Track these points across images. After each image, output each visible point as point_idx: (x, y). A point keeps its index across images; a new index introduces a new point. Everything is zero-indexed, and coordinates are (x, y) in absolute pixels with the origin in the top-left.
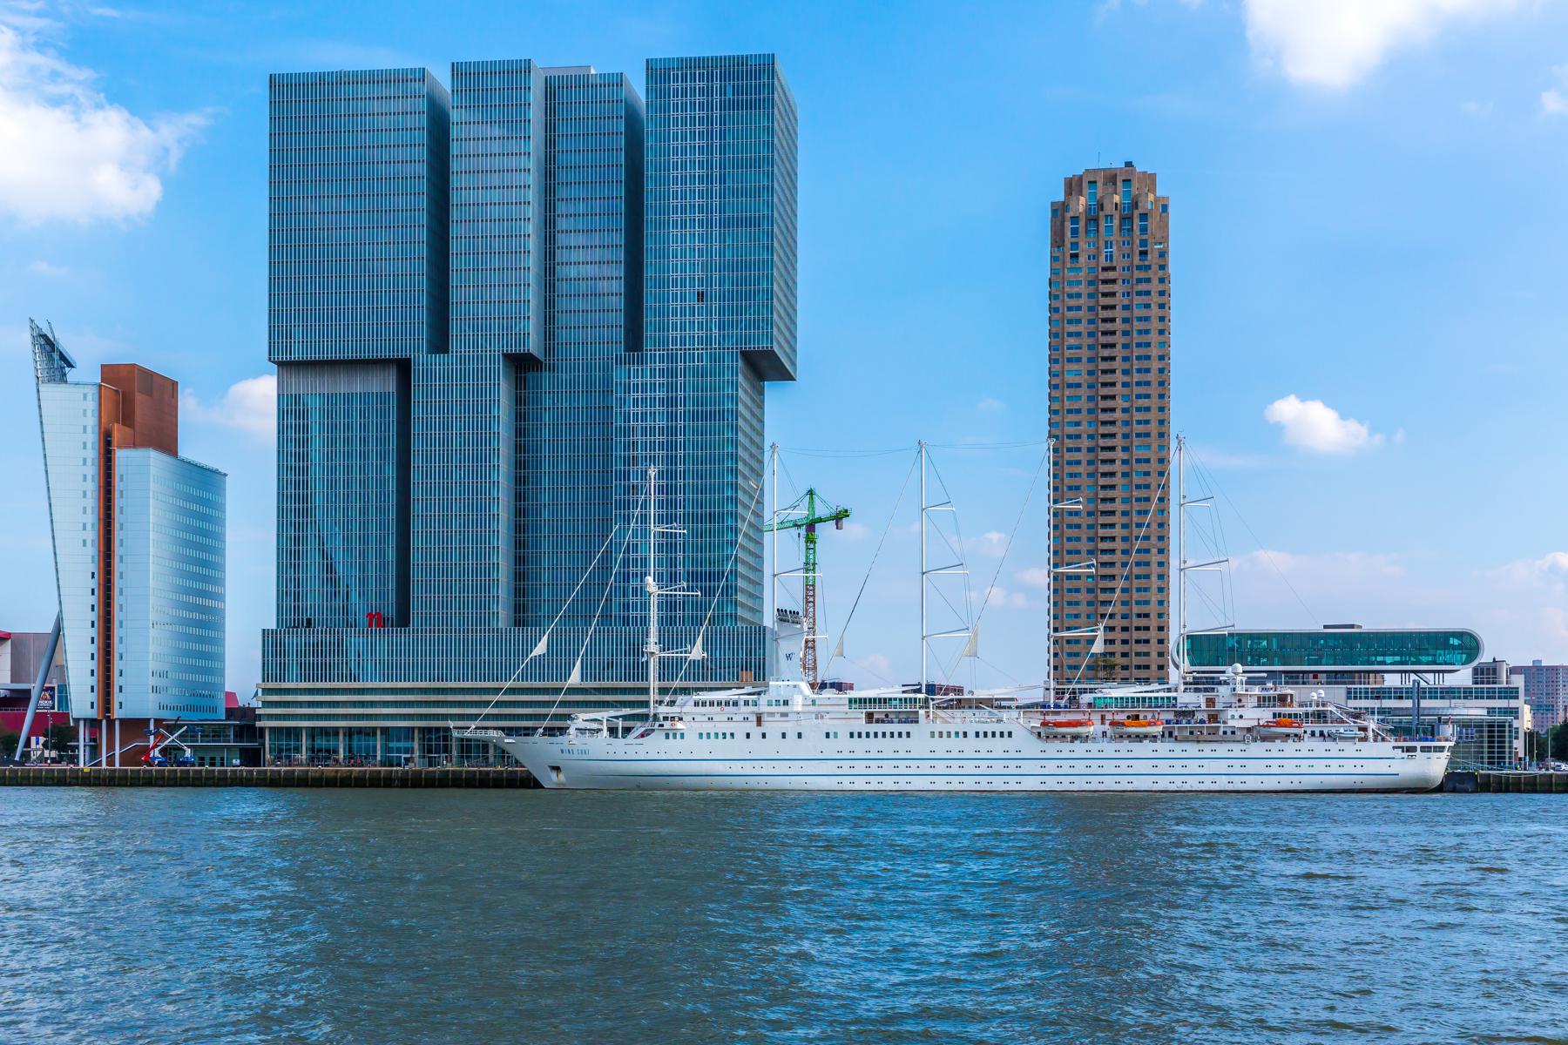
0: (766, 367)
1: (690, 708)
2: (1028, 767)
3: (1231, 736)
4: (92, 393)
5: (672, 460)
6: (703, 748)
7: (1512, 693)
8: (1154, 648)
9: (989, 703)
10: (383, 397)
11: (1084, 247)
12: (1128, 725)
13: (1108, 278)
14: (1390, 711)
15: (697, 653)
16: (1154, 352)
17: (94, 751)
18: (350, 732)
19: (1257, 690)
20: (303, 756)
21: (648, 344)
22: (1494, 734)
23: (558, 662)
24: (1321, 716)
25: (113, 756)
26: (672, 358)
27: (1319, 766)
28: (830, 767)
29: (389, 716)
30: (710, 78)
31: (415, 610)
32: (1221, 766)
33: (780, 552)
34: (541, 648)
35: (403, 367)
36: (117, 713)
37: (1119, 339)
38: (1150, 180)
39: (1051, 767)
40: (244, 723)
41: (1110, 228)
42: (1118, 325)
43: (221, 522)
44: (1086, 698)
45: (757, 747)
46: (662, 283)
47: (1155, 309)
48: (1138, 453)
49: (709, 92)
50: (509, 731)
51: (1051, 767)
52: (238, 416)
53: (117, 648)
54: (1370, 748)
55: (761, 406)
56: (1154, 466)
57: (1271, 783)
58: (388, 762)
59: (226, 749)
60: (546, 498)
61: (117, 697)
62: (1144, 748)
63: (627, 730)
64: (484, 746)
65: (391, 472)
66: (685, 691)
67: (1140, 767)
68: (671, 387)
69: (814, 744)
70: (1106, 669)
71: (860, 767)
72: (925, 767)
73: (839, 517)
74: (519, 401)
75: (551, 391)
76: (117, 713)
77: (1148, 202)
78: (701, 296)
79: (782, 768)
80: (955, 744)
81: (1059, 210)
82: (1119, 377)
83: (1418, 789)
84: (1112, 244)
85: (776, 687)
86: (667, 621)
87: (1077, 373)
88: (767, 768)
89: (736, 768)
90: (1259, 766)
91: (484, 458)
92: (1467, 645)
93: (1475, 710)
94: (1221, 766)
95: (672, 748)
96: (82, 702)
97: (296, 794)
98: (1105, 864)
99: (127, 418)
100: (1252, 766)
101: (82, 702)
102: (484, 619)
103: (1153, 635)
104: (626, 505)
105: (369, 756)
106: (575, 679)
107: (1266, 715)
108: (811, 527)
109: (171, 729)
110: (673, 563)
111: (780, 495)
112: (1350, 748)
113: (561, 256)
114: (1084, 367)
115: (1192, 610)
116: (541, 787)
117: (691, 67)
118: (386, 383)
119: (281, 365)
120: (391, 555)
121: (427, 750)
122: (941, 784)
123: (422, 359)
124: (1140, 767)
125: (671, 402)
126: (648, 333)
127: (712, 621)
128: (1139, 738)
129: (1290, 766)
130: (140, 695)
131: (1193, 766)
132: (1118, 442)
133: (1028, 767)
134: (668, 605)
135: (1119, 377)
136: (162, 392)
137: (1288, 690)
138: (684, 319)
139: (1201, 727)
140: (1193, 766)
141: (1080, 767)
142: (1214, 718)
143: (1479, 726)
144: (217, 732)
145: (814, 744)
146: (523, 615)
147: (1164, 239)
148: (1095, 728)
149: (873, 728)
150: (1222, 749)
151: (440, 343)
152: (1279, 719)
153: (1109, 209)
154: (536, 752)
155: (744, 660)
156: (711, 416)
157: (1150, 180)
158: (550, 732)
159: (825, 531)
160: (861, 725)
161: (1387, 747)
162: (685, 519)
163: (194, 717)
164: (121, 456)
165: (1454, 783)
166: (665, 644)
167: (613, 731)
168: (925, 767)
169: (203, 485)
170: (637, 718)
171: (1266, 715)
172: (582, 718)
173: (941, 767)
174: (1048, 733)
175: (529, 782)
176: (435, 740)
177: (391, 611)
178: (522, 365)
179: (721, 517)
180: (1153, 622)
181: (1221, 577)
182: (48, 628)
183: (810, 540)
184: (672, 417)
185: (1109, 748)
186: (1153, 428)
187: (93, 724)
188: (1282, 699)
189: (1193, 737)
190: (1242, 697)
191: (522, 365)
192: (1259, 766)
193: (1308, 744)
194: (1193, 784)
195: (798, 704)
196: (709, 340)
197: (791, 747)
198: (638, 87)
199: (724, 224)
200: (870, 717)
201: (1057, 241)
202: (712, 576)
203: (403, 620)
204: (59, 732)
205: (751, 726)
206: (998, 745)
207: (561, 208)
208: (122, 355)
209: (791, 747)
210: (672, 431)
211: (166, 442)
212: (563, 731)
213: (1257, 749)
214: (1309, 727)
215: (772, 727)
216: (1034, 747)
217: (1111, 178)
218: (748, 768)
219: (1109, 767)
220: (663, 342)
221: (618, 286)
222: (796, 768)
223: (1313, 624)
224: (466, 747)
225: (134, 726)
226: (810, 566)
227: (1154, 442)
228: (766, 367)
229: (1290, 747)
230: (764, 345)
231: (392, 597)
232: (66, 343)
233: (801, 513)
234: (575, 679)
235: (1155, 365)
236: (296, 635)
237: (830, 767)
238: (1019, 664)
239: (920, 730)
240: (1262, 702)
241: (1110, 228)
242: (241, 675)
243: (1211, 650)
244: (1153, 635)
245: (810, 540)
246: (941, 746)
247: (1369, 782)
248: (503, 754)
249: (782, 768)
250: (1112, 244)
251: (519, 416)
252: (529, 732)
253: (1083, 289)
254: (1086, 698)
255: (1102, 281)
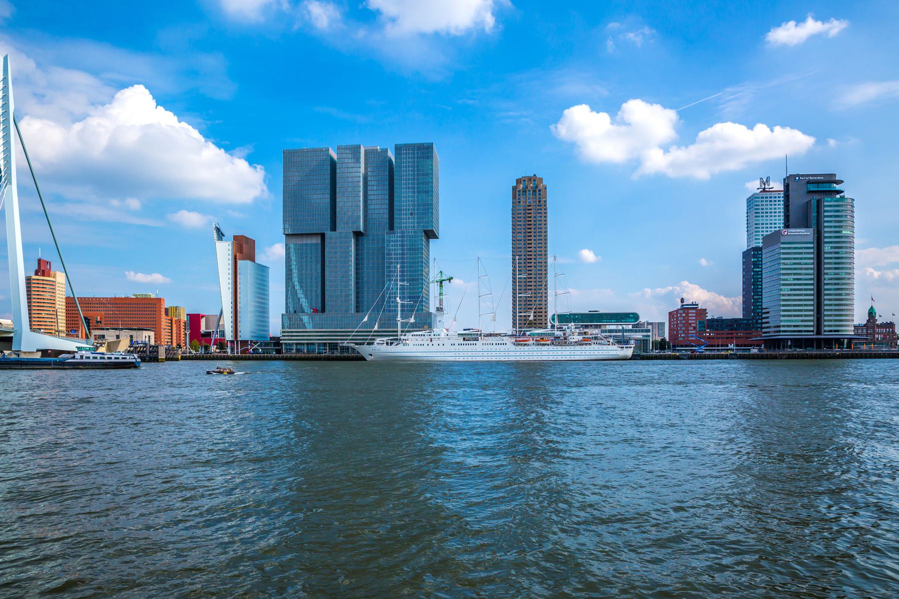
0: (430, 234)
1: (410, 337)
2: (511, 354)
3: (571, 344)
4: (230, 243)
5: (403, 263)
6: (415, 349)
7: (648, 331)
8: (544, 318)
9: (500, 335)
10: (317, 244)
11: (522, 200)
12: (541, 341)
13: (529, 207)
14: (616, 336)
15: (412, 320)
16: (543, 230)
17: (232, 350)
18: (308, 344)
19: (578, 330)
20: (294, 351)
21: (396, 229)
22: (643, 343)
23: (371, 323)
24: (596, 338)
25: (238, 352)
26: (403, 232)
27: (596, 353)
28: (452, 354)
29: (316, 340)
30: (414, 150)
31: (327, 307)
32: (568, 353)
33: (434, 289)
34: (366, 319)
35: (323, 236)
36: (239, 339)
37: (532, 226)
38: (541, 180)
39: (518, 354)
40: (276, 341)
41: (530, 194)
42: (532, 222)
43: (268, 282)
44: (528, 333)
45: (431, 348)
46: (400, 210)
47: (543, 218)
48: (538, 260)
49: (413, 154)
50: (356, 344)
51: (518, 354)
52: (274, 253)
53: (239, 319)
54: (611, 347)
55: (428, 246)
56: (543, 264)
57: (582, 358)
58: (319, 353)
59: (271, 350)
60: (365, 274)
61: (239, 334)
62: (545, 348)
63: (391, 344)
64: (348, 348)
65: (319, 266)
66: (409, 332)
67: (544, 353)
68: (402, 241)
69: (448, 347)
70: (531, 325)
71: (461, 354)
72: (481, 354)
73: (450, 279)
74: (357, 245)
75: (368, 245)
76: (239, 339)
77: (541, 187)
78: (411, 214)
79: (438, 354)
80: (490, 347)
81: (514, 189)
82: (533, 238)
83: (625, 359)
84: (530, 199)
85: (436, 330)
86: (402, 311)
87: (520, 236)
88: (434, 354)
89: (425, 354)
90: (579, 353)
91: (347, 262)
92: (635, 317)
93: (639, 336)
94: (568, 353)
95: (405, 349)
96: (229, 336)
97: (294, 363)
98: (529, 383)
99: (241, 252)
100: (577, 353)
101: (229, 336)
102: (347, 311)
103: (543, 314)
104: (389, 276)
105: (313, 351)
106: (376, 328)
107: (581, 338)
108: (441, 282)
109: (255, 343)
110: (403, 293)
111: (433, 274)
112: (605, 347)
113: (369, 202)
114: (523, 235)
115: (555, 307)
116: (365, 360)
117: (407, 146)
118: (317, 240)
119: (287, 235)
120: (319, 291)
121: (331, 349)
122: (461, 359)
123: (328, 233)
124: (544, 353)
125: (403, 245)
126: (396, 225)
127: (418, 310)
128: (544, 345)
129: (588, 353)
130: (246, 333)
131: (559, 353)
132: (533, 257)
133: (511, 354)
134: (403, 306)
135: (533, 238)
136: (251, 243)
137: (586, 330)
138: (406, 222)
139: (562, 341)
140: (559, 353)
141: (526, 353)
142: (565, 339)
143: (640, 340)
144: (267, 344)
145: (448, 347)
146: (358, 309)
147: (546, 197)
148: (531, 342)
149: (465, 342)
150: (568, 348)
151: (334, 228)
152: (585, 339)
153: (529, 188)
154: (364, 350)
155: (425, 323)
156: (415, 249)
157: (541, 180)
158: (368, 344)
159: (445, 283)
160: (462, 341)
161: (616, 347)
162: (407, 280)
163: (262, 340)
164: (239, 262)
165: (634, 357)
166: (403, 318)
167: (387, 344)
168: (481, 354)
169: (262, 271)
170: (395, 340)
171: (581, 338)
172: (378, 340)
173: (485, 354)
174: (517, 343)
175: (363, 359)
176: (333, 346)
177: (319, 308)
178: (358, 235)
179: (418, 280)
180: (543, 310)
181: (564, 296)
182: (219, 314)
183: (441, 286)
184: (403, 250)
185: (535, 348)
186: (543, 253)
187: (232, 342)
188: (585, 333)
189: (559, 344)
190: (573, 331)
191: (358, 235)
192: (579, 353)
193: (593, 346)
194: (560, 358)
195: (443, 335)
196: (414, 227)
197: (441, 348)
198: (391, 154)
199: (419, 192)
200: (464, 339)
201: (514, 197)
202: (416, 297)
203: (323, 310)
204: (221, 344)
205: (429, 342)
206: (502, 347)
207: (369, 188)
208: (239, 233)
209: (441, 348)
210: (403, 254)
211: (252, 258)
212: (373, 343)
213: (578, 348)
214: (593, 341)
215: (435, 342)
216: (513, 348)
217: (530, 179)
218: (428, 354)
219: (535, 353)
220: (400, 228)
221: (387, 211)
222: (442, 354)
223: (586, 311)
224: (343, 348)
225: (244, 343)
226: (441, 294)
227: (543, 256)
228: (430, 234)
229: (588, 347)
230: (430, 228)
231: (320, 305)
232: (223, 230)
233: (438, 279)
234: (376, 328)
235: (544, 234)
236: (292, 313)
237: (452, 354)
238: (505, 325)
239: (479, 343)
240: (580, 334)
241: (530, 194)
242: (275, 328)
243: (564, 318)
244: (543, 314)
245: (441, 286)
246: (485, 348)
247: (610, 357)
248: (353, 349)
249: (438, 354)
250: (530, 199)
251: (357, 250)
252: (363, 344)
253: (522, 212)
254: (528, 333)
255: (527, 209)
